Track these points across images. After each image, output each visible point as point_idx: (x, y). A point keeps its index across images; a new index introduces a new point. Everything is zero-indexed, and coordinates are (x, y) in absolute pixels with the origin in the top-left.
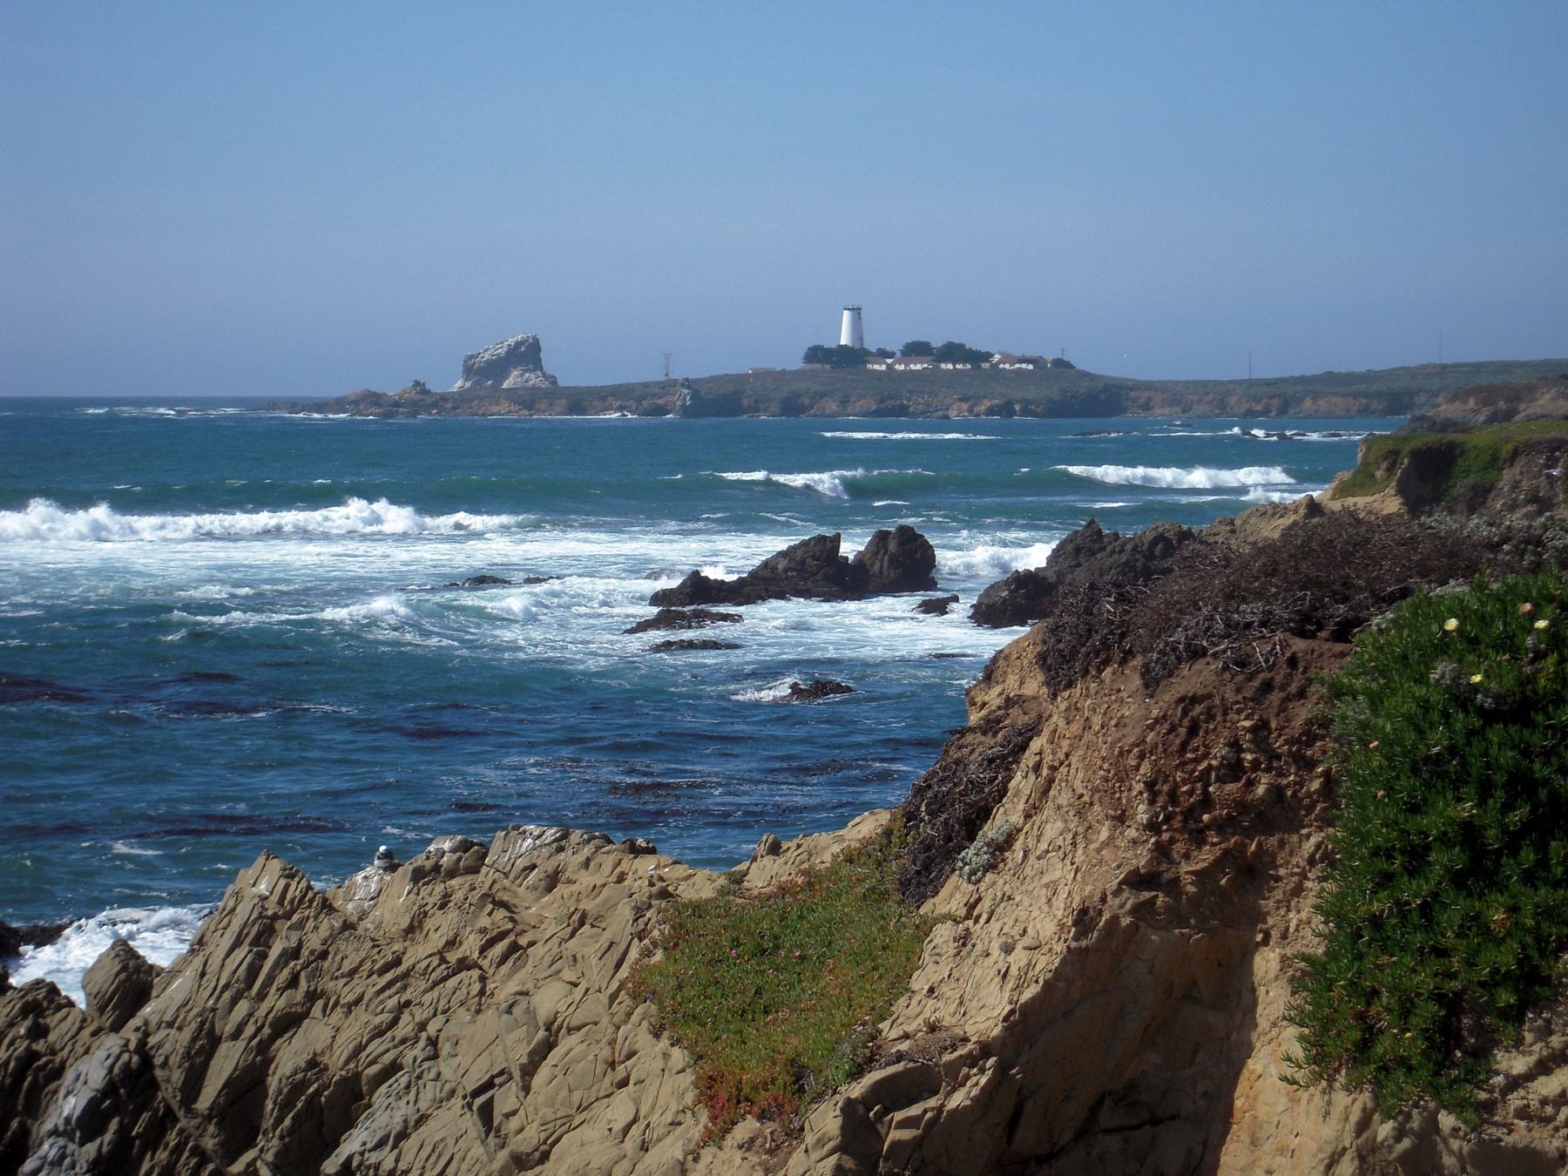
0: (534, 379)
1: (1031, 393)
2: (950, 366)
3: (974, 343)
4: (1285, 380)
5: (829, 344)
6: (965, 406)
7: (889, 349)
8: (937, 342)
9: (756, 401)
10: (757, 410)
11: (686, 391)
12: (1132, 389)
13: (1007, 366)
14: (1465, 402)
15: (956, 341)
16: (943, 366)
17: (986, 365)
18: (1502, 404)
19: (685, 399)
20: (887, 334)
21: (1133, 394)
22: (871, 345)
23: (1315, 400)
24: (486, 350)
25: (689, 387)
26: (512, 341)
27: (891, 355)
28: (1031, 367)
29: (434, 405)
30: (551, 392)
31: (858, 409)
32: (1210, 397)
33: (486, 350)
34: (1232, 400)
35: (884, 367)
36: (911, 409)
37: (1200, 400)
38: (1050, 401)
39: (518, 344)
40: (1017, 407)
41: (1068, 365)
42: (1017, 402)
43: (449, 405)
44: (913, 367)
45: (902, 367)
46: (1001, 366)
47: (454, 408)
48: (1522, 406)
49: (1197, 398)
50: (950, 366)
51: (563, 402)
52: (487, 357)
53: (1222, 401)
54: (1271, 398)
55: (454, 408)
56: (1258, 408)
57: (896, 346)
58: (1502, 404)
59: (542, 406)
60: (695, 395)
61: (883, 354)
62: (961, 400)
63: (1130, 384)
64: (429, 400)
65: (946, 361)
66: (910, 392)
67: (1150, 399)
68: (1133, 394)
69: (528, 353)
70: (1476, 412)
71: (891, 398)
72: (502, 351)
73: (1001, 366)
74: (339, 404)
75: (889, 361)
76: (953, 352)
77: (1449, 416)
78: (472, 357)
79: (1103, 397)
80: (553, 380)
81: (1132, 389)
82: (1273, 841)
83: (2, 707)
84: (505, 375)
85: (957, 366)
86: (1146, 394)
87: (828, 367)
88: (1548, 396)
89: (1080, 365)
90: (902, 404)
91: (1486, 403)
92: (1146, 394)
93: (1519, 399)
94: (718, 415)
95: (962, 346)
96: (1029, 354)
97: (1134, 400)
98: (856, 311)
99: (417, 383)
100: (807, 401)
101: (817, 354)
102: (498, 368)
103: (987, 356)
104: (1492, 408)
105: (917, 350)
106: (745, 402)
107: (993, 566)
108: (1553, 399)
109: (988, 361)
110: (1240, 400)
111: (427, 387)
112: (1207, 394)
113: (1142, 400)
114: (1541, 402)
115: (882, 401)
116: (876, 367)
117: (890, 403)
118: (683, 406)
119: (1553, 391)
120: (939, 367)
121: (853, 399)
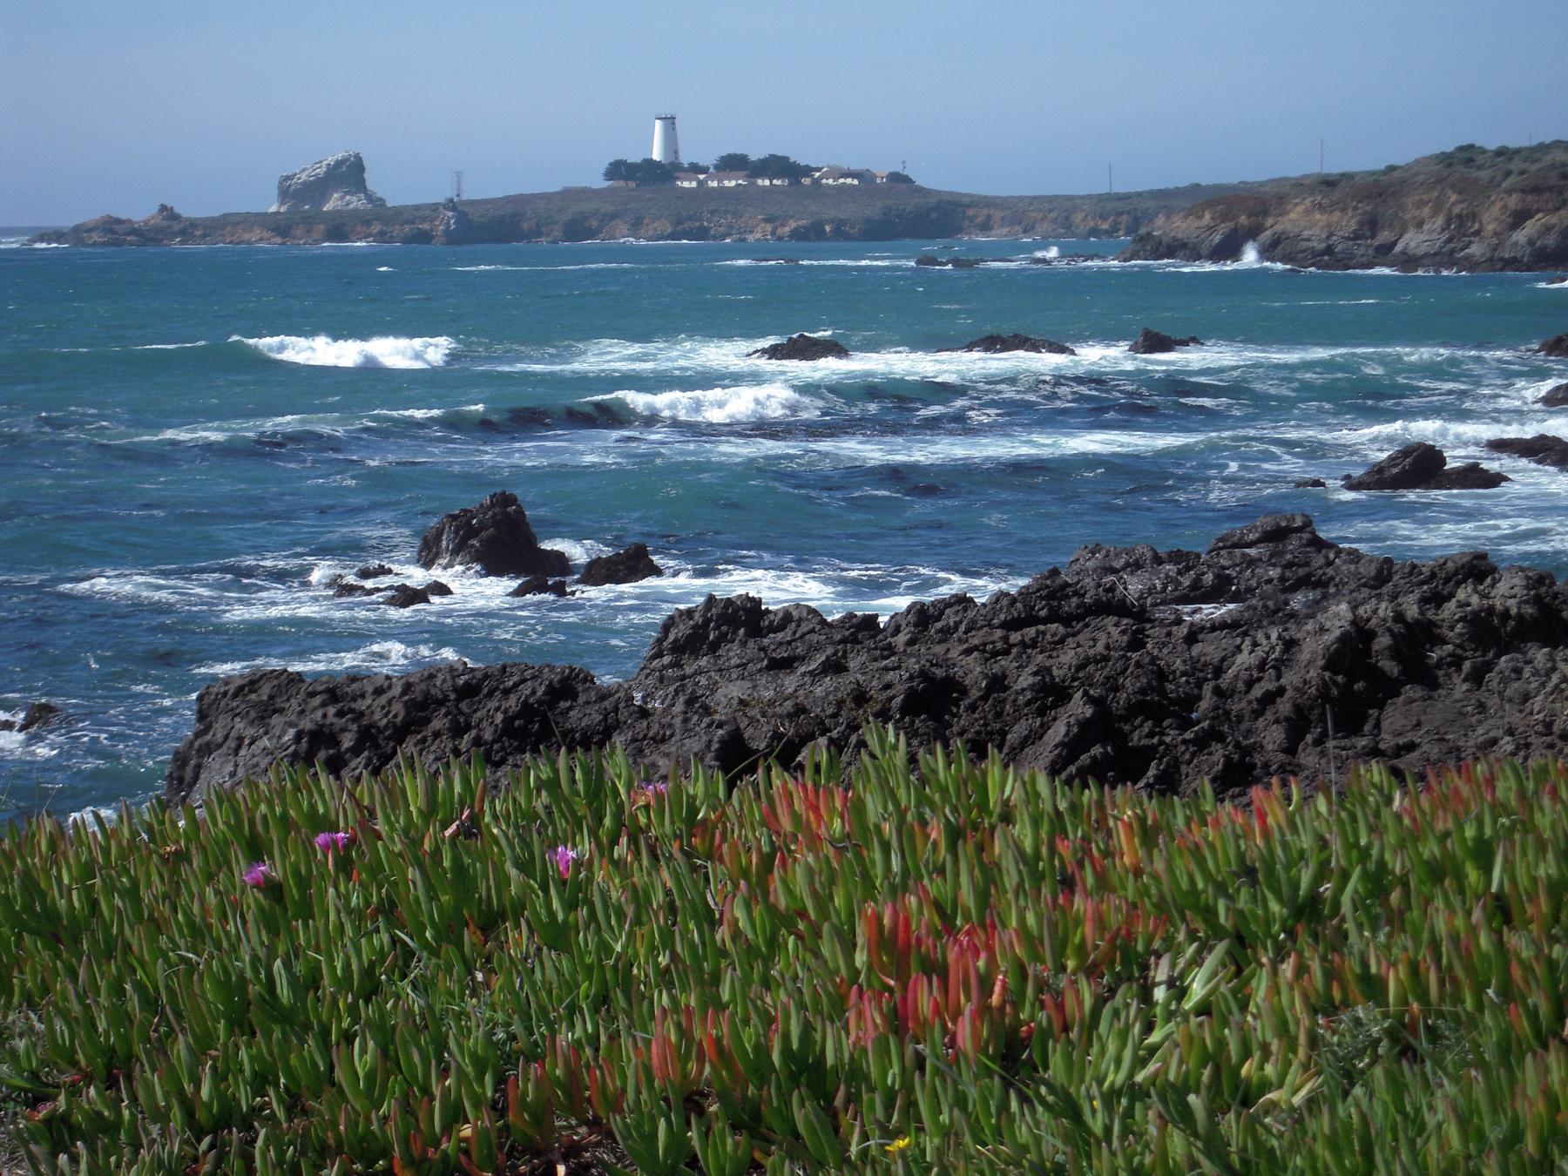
0: (356, 202)
1: (848, 211)
2: (767, 182)
3: (800, 157)
4: (1139, 194)
5: (634, 157)
6: (769, 228)
7: (701, 163)
8: (755, 155)
9: (537, 225)
10: (539, 234)
11: (450, 214)
12: (969, 206)
13: (830, 181)
14: (1201, 217)
15: (780, 154)
16: (760, 182)
17: (806, 181)
18: (1243, 220)
19: (448, 224)
20: (701, 149)
21: (971, 212)
22: (685, 160)
23: (1168, 217)
24: (303, 170)
25: (454, 208)
26: (331, 160)
27: (704, 170)
28: (856, 182)
29: (182, 232)
30: (380, 218)
31: (651, 233)
32: (1053, 215)
33: (303, 170)
34: (1078, 218)
35: (694, 184)
36: (712, 232)
37: (1044, 218)
38: (868, 220)
39: (339, 163)
40: (828, 229)
41: (907, 180)
42: (828, 222)
43: (198, 233)
44: (726, 183)
45: (715, 184)
46: (824, 181)
47: (204, 236)
48: (1270, 221)
49: (1041, 215)
50: (767, 182)
51: (322, 227)
52: (304, 177)
53: (1067, 219)
54: (1121, 214)
55: (204, 236)
56: (1105, 226)
57: (708, 158)
58: (1243, 220)
59: (299, 232)
60: (462, 218)
61: (696, 169)
62: (766, 220)
63: (966, 200)
64: (177, 227)
65: (762, 176)
66: (712, 212)
67: (989, 217)
68: (971, 212)
69: (350, 173)
70: (1211, 229)
71: (690, 218)
72: (321, 171)
73: (824, 181)
74: (58, 235)
75: (702, 177)
76: (777, 166)
77: (1180, 235)
78: (287, 178)
79: (934, 215)
80: (378, 203)
81: (969, 206)
82: (1138, 685)
83: (1564, 382)
84: (324, 198)
85: (775, 182)
86: (985, 211)
87: (632, 184)
88: (1300, 208)
89: (921, 180)
90: (701, 226)
91: (1224, 218)
92: (985, 211)
93: (1265, 213)
94: (492, 241)
95: (786, 159)
96: (855, 166)
97: (972, 219)
98: (670, 121)
99: (163, 208)
100: (594, 224)
101: (618, 170)
102: (318, 188)
103: (807, 171)
104: (1230, 225)
105: (733, 163)
106: (525, 226)
107: (784, 407)
108: (1307, 212)
109: (807, 176)
110: (1086, 216)
111: (177, 210)
112: (1051, 211)
113: (980, 219)
114: (1292, 215)
115: (679, 222)
116: (686, 184)
117: (687, 225)
118: (447, 232)
119: (1308, 202)
120: (755, 183)
121: (646, 221)
